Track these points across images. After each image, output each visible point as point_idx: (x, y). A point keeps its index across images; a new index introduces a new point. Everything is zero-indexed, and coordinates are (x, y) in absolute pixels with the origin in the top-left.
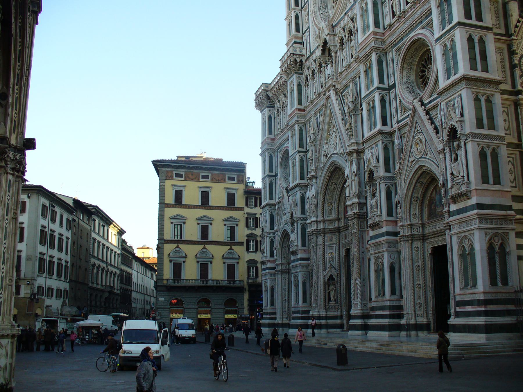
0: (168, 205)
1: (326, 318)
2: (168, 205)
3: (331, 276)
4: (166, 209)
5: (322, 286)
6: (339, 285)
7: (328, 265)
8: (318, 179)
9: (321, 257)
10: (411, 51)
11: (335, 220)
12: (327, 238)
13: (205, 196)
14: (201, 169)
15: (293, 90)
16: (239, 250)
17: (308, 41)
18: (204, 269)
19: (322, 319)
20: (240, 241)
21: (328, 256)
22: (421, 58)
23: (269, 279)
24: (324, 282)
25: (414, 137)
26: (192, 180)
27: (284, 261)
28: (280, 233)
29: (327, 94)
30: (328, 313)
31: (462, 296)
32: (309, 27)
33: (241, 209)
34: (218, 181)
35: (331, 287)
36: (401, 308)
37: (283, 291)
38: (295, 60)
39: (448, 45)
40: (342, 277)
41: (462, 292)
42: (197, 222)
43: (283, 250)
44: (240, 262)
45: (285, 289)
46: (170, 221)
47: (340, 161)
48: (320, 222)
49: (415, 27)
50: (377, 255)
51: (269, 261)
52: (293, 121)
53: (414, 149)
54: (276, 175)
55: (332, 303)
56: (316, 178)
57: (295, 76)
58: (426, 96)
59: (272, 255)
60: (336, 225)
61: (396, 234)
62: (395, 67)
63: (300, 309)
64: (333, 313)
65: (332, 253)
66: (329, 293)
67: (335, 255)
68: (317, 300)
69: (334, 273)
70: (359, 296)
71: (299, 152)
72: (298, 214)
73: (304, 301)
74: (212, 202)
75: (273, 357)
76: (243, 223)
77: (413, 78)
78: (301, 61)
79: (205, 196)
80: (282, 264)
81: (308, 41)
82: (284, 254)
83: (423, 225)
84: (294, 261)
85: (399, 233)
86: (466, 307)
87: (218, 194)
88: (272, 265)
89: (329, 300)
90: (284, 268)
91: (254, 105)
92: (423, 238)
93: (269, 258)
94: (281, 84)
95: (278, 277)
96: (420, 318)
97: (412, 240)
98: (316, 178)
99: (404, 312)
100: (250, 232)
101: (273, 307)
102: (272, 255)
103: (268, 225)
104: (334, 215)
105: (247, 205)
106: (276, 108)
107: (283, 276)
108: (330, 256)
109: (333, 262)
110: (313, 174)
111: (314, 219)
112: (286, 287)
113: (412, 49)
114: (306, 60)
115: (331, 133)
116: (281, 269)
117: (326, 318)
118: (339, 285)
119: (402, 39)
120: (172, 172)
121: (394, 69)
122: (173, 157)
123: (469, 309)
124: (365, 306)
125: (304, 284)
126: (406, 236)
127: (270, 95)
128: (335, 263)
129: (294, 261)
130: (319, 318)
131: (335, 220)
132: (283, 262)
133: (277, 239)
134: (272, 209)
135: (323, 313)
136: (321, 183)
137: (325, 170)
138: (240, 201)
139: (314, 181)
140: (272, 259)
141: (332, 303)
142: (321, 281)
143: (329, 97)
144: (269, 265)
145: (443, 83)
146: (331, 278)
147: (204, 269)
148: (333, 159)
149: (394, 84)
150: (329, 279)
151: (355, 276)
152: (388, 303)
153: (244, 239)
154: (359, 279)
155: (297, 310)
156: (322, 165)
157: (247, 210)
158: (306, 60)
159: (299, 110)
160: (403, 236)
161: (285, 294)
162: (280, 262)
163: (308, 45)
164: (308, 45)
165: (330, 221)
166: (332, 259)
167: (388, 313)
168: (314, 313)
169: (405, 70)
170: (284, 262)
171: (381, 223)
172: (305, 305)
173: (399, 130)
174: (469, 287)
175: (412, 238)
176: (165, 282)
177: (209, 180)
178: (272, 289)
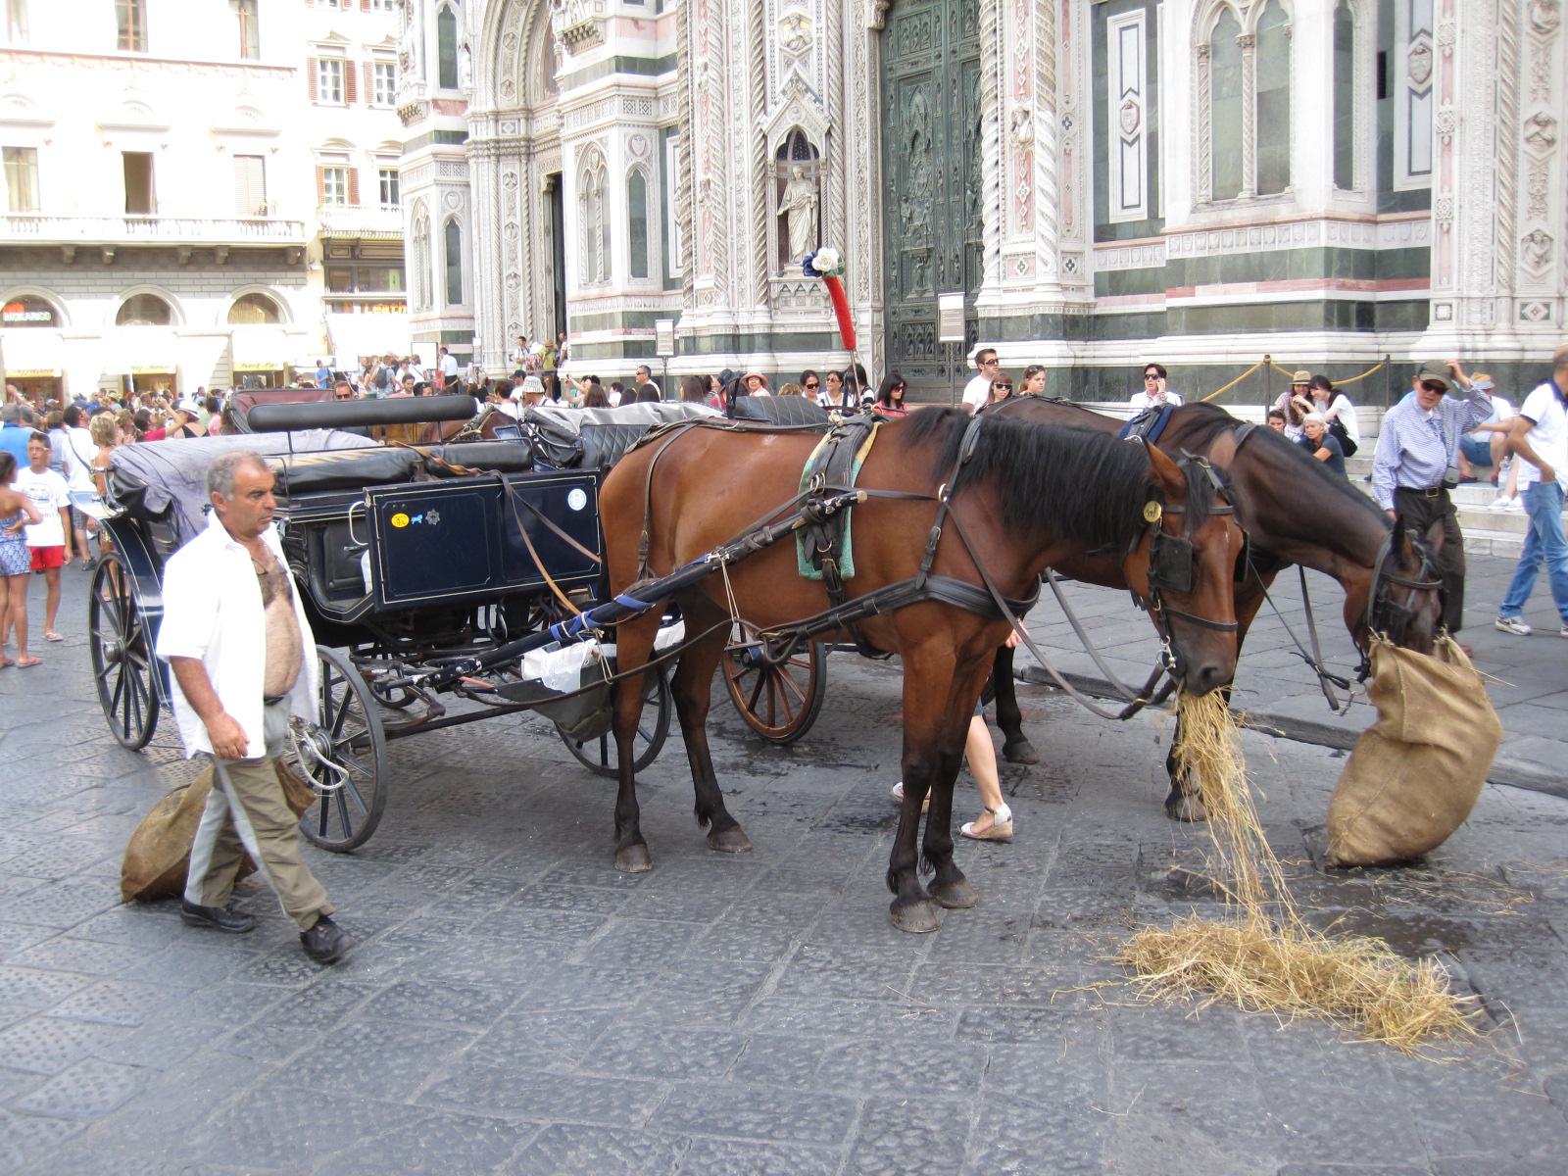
1: (773, 342)
5: (748, 185)
6: (836, 178)
7: (779, 79)
9: (744, 40)
19: (751, 350)
21: (779, 35)
23: (620, 124)
27: (510, 102)
30: (780, 319)
31: (1213, 239)
35: (799, 192)
36: (1414, 264)
37: (506, 235)
40: (851, 140)
41: (1206, 218)
43: (504, 50)
45: (512, 226)
50: (586, 140)
51: (436, 103)
59: (448, 78)
61: (459, 137)
64: (803, 319)
65: (800, 19)
66: (783, 220)
67: (817, 29)
68: (721, 253)
73: (638, 268)
75: (974, 614)
80: (497, 116)
82: (508, 70)
83: (529, 114)
84: (577, 79)
85: (465, 135)
86: (1199, 289)
88: (450, 123)
89: (784, 253)
90: (508, 135)
93: (433, 89)
95: (482, 174)
96: (1536, 326)
97: (498, 156)
99: (1435, 293)
101: (456, 310)
102: (448, 78)
107: (505, 170)
108: (787, 34)
109: (805, 64)
112: (517, 221)
116: (492, 136)
117: (773, 342)
118: (836, 178)
123: (1207, 295)
124: (1070, 265)
125: (636, 186)
126: (482, 143)
128: (816, 71)
129: (577, 79)
130: (735, 342)
132: (503, 106)
135: (754, 319)
140: (448, 94)
142: (744, 163)
146: (798, 145)
150: (782, 153)
151: (1012, 105)
152: (1322, 237)
154: (1047, 115)
155: (595, 309)
160: (475, 143)
161: (513, 250)
162: (491, 107)
166: (799, 50)
167: (1321, 294)
168: (707, 317)
170: (505, 104)
171: (599, 27)
172: (638, 285)
174: (1244, 195)
178: (452, 229)
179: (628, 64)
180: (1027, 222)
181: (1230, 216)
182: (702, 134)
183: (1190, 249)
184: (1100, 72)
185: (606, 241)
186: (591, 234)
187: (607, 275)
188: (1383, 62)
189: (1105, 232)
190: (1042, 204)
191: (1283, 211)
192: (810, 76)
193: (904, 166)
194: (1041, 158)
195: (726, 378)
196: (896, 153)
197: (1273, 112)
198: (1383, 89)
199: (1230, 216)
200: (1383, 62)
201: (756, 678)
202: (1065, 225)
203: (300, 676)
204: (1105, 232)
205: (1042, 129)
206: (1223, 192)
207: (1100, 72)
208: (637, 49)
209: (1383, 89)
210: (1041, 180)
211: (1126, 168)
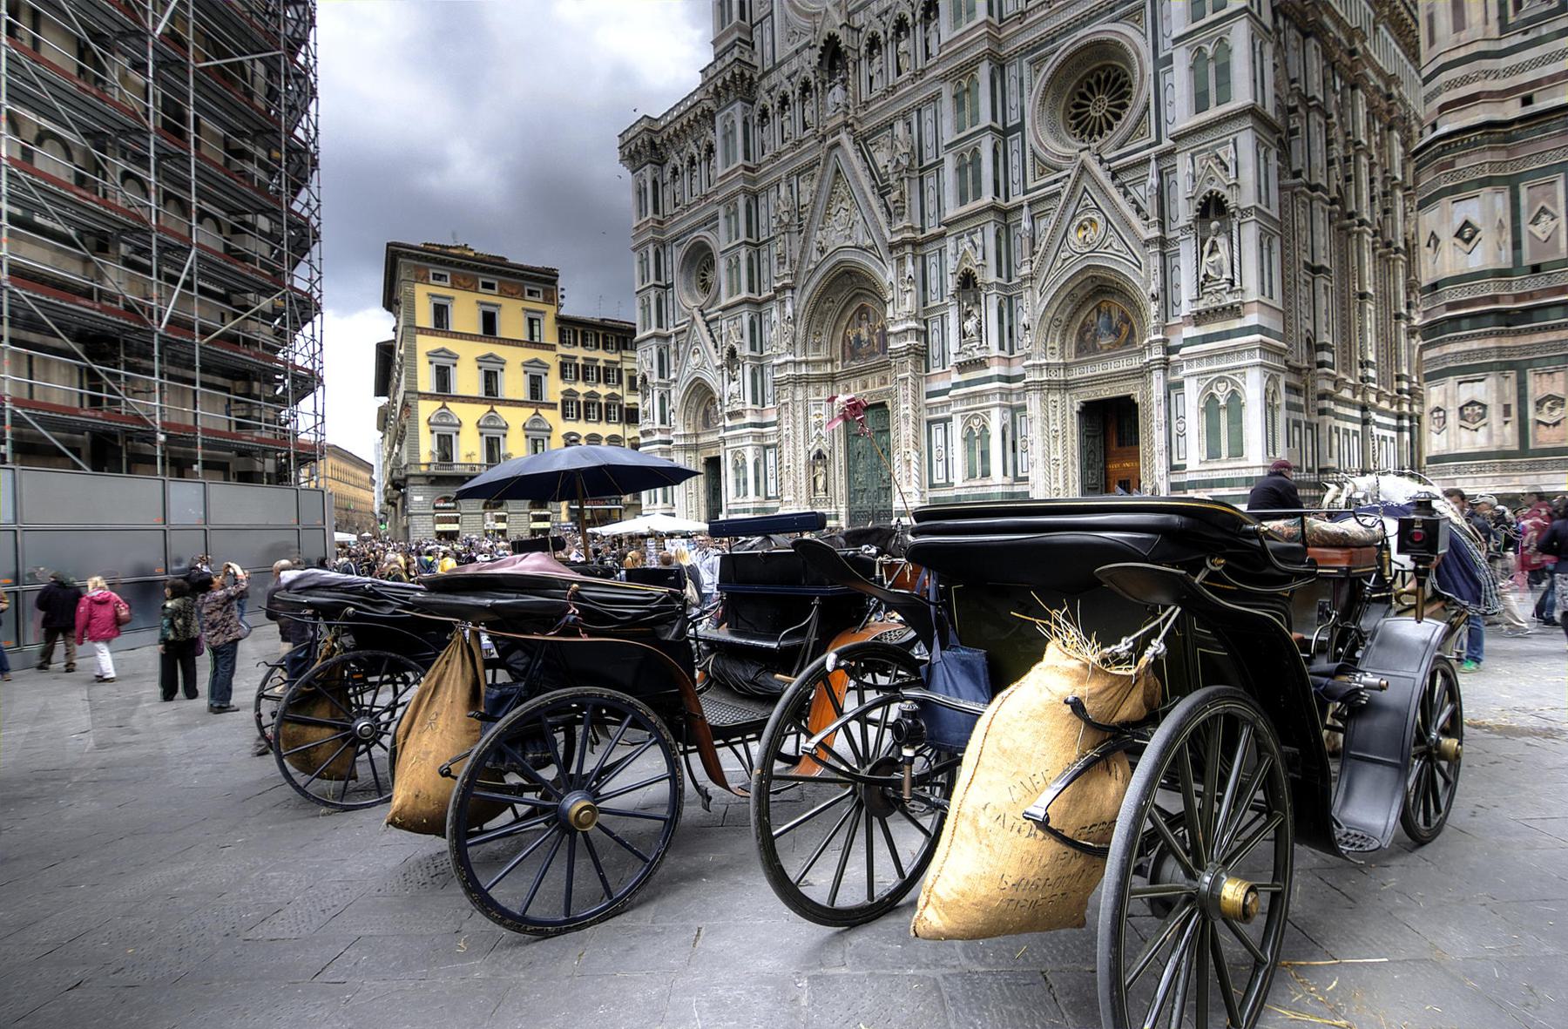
0: (423, 331)
2: (423, 331)
3: (819, 452)
4: (420, 338)
8: (798, 292)
10: (1069, 65)
11: (826, 362)
12: (811, 390)
13: (489, 322)
14: (483, 270)
15: (733, 132)
16: (552, 417)
17: (768, 39)
18: (445, 444)
20: (551, 400)
21: (813, 420)
22: (1080, 81)
24: (808, 462)
25: (1074, 216)
26: (465, 289)
28: (683, 384)
29: (830, 141)
32: (771, 13)
33: (551, 347)
34: (511, 296)
35: (820, 469)
38: (742, 74)
39: (1209, 50)
42: (476, 365)
44: (553, 435)
46: (427, 359)
47: (868, 262)
48: (800, 363)
49: (1099, 15)
52: (736, 187)
53: (1072, 236)
54: (667, 287)
55: (821, 494)
56: (793, 289)
57: (738, 105)
58: (1111, 145)
60: (828, 369)
61: (669, 442)
62: (1026, 92)
63: (751, 506)
69: (825, 446)
70: (914, 478)
71: (746, 243)
72: (744, 350)
73: (757, 494)
74: (503, 331)
76: (555, 372)
77: (1059, 116)
78: (751, 78)
79: (489, 322)
81: (768, 39)
87: (511, 319)
88: (664, 437)
91: (618, 156)
92: (1066, 386)
93: (658, 425)
94: (696, 117)
98: (793, 289)
100: (567, 387)
103: (656, 370)
104: (823, 354)
105: (562, 341)
106: (668, 170)
110: (787, 281)
111: (791, 358)
113: (1075, 61)
114: (761, 78)
115: (833, 211)
119: (1053, 40)
120: (427, 269)
121: (1022, 96)
122: (419, 243)
127: (658, 141)
131: (826, 362)
133: (677, 394)
134: (662, 343)
136: (805, 298)
137: (818, 277)
138: (549, 333)
139: (789, 294)
141: (821, 494)
142: (802, 460)
143: (837, 145)
144: (658, 437)
145: (1181, 115)
146: (819, 455)
147: (445, 444)
148: (840, 257)
149: (1022, 124)
153: (558, 399)
156: (812, 267)
157: (562, 350)
158: (761, 78)
159: (746, 168)
163: (768, 49)
164: (768, 49)
165: (816, 364)
169: (1049, 99)
173: (1030, 205)
175: (1048, 387)
176: (424, 469)
177: (496, 292)
179: (754, 425)
180: (909, 483)
181: (974, 483)
182: (787, 451)
183: (1195, 477)
184: (930, 440)
185: (745, 483)
186: (737, 481)
187: (746, 494)
188: (1014, 443)
189: (932, 486)
190: (914, 478)
191: (989, 482)
192: (823, 433)
193: (855, 461)
194: (913, 465)
195: (1108, 490)
196: (852, 459)
197: (985, 456)
198: (1014, 450)
199: (974, 483)
200: (1014, 443)
201: (566, 854)
202: (920, 484)
203: (324, 810)
204: (932, 486)
205: (914, 456)
206: (972, 476)
207: (930, 440)
208: (756, 419)
209: (1014, 450)
210: (914, 472)
211: (939, 469)
